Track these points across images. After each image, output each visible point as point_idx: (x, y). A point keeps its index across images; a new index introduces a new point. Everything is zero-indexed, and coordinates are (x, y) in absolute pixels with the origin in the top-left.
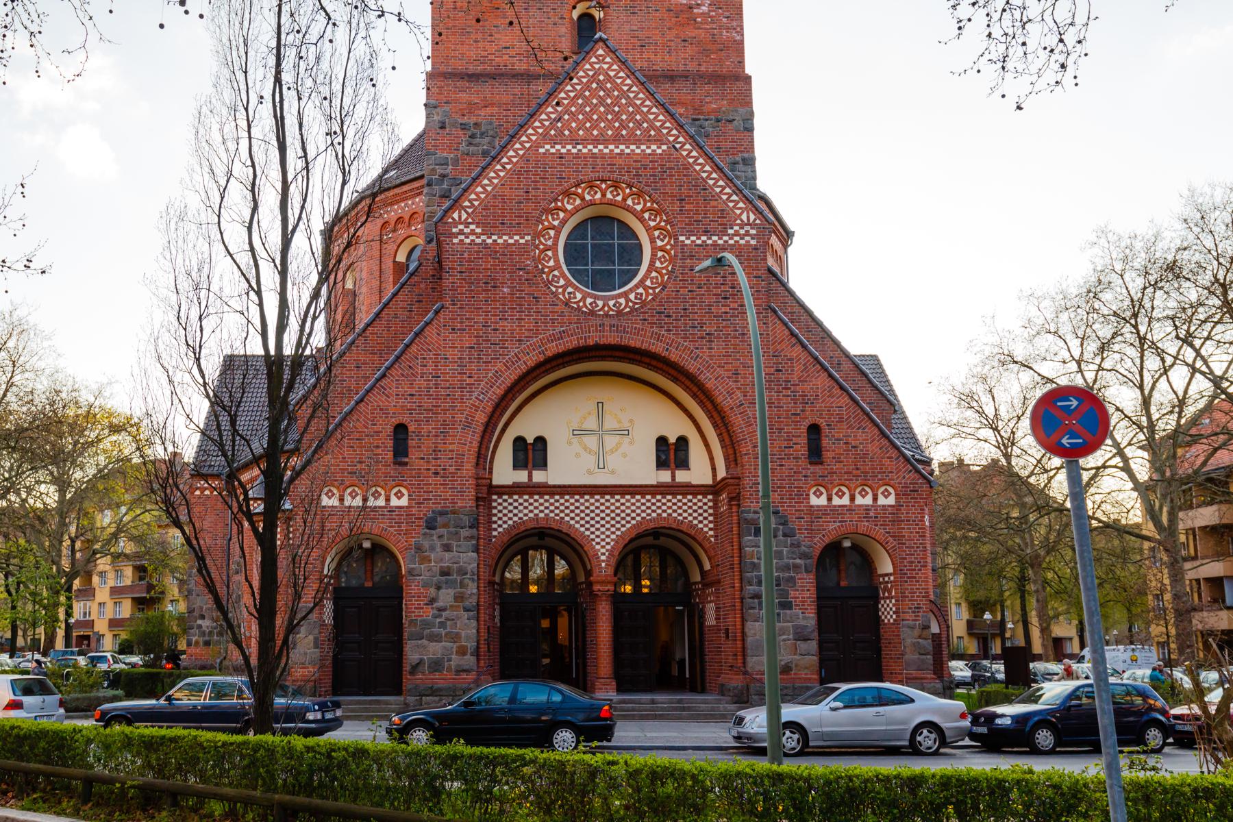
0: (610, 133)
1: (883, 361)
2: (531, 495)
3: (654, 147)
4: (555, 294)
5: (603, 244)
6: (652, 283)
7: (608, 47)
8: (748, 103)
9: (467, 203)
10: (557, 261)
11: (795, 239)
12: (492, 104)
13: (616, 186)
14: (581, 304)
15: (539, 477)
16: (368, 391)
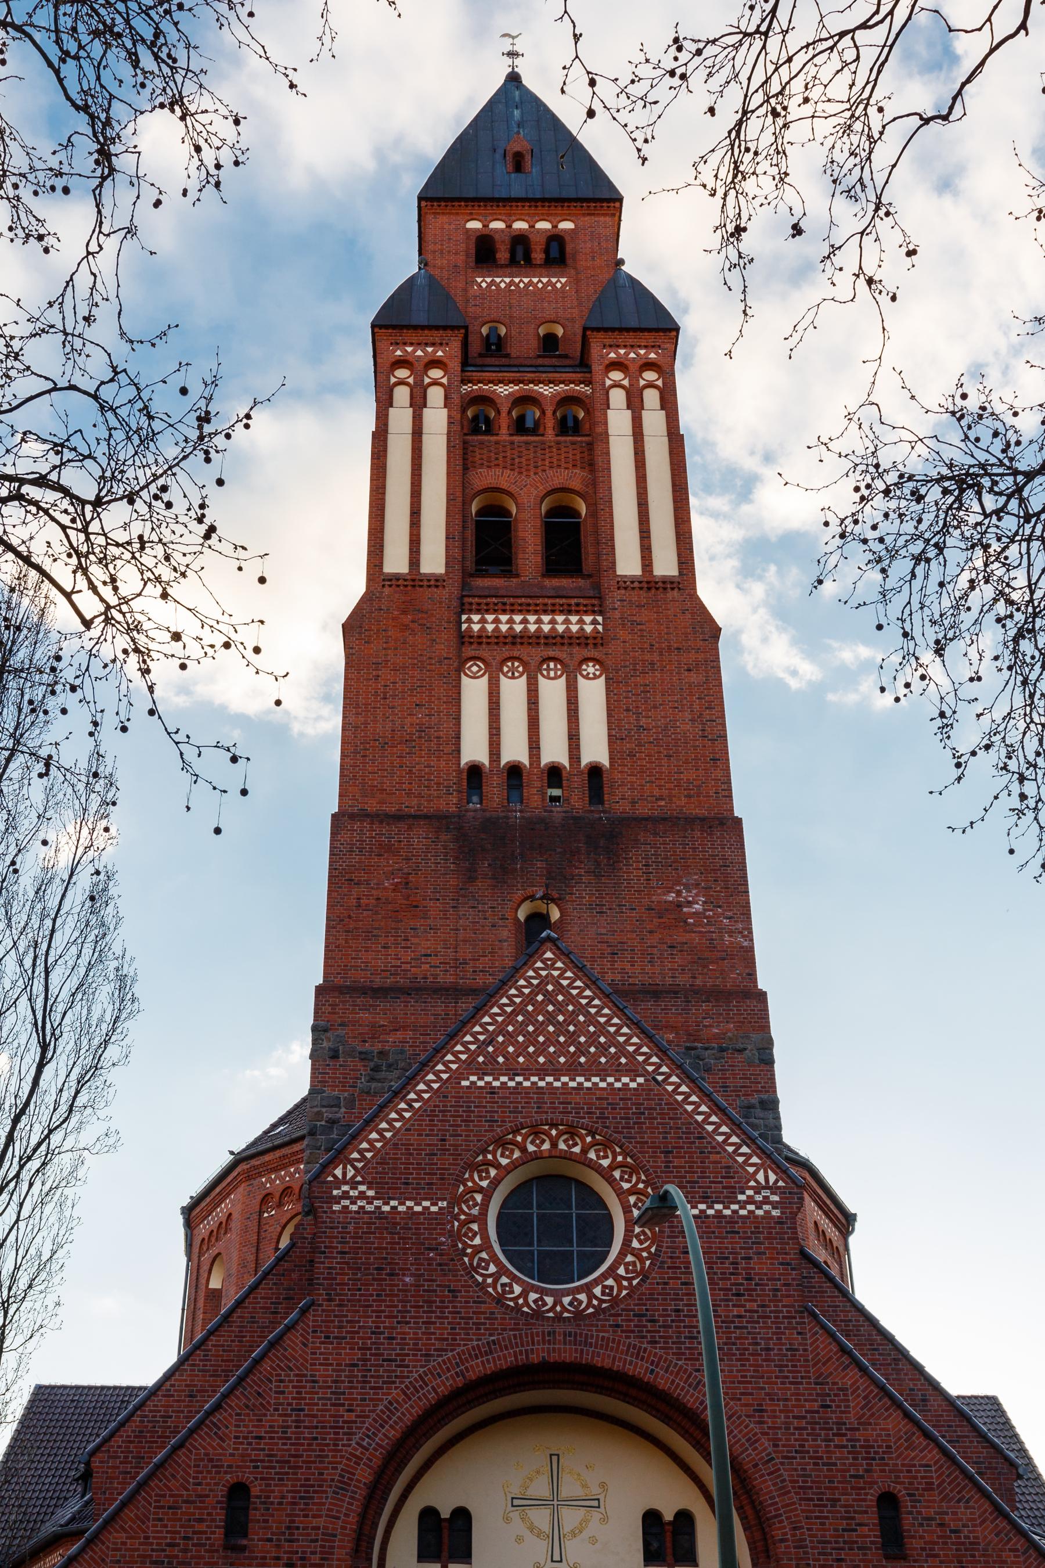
0: (562, 1060)
1: (1006, 1406)
3: (625, 1080)
4: (483, 1286)
5: (556, 1215)
6: (627, 1271)
7: (559, 948)
8: (764, 1026)
9: (355, 1155)
10: (485, 1237)
11: (857, 1225)
12: (405, 1028)
13: (572, 1132)
14: (521, 1301)
16: (192, 1431)
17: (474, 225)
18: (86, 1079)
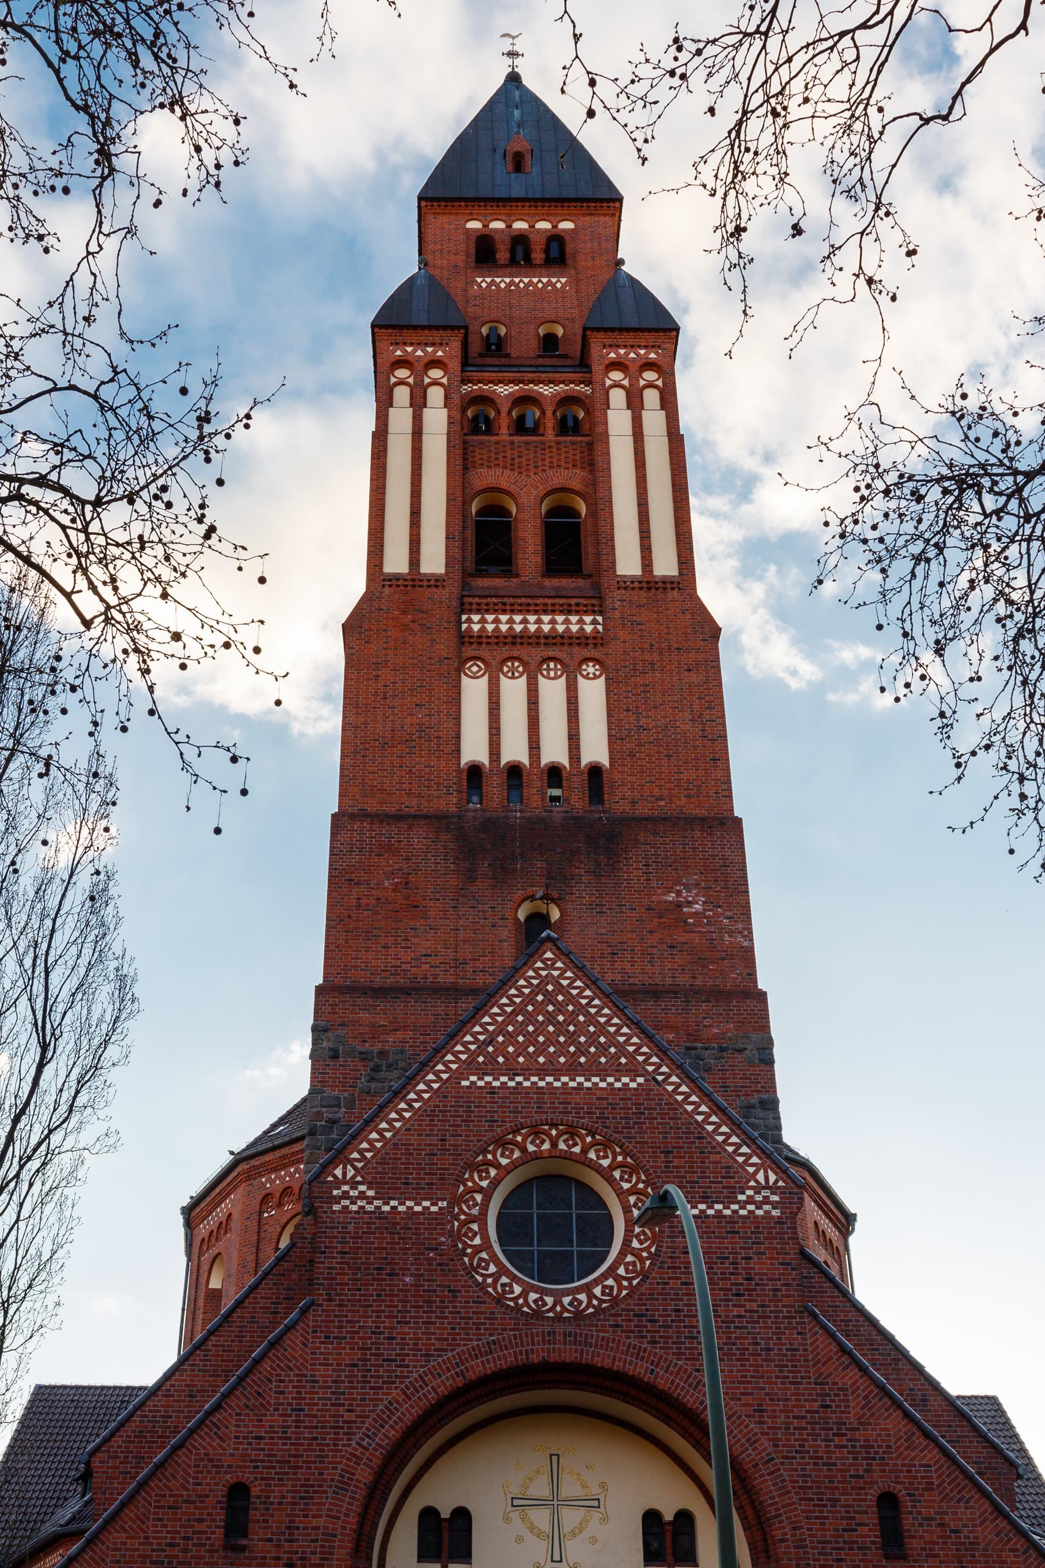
0: (562, 1060)
1: (1006, 1406)
3: (625, 1080)
4: (483, 1286)
5: (556, 1215)
6: (627, 1271)
7: (559, 948)
8: (764, 1026)
9: (355, 1155)
10: (485, 1237)
11: (857, 1225)
12: (405, 1028)
13: (572, 1132)
14: (521, 1301)
16: (192, 1431)
17: (474, 225)
18: (86, 1079)
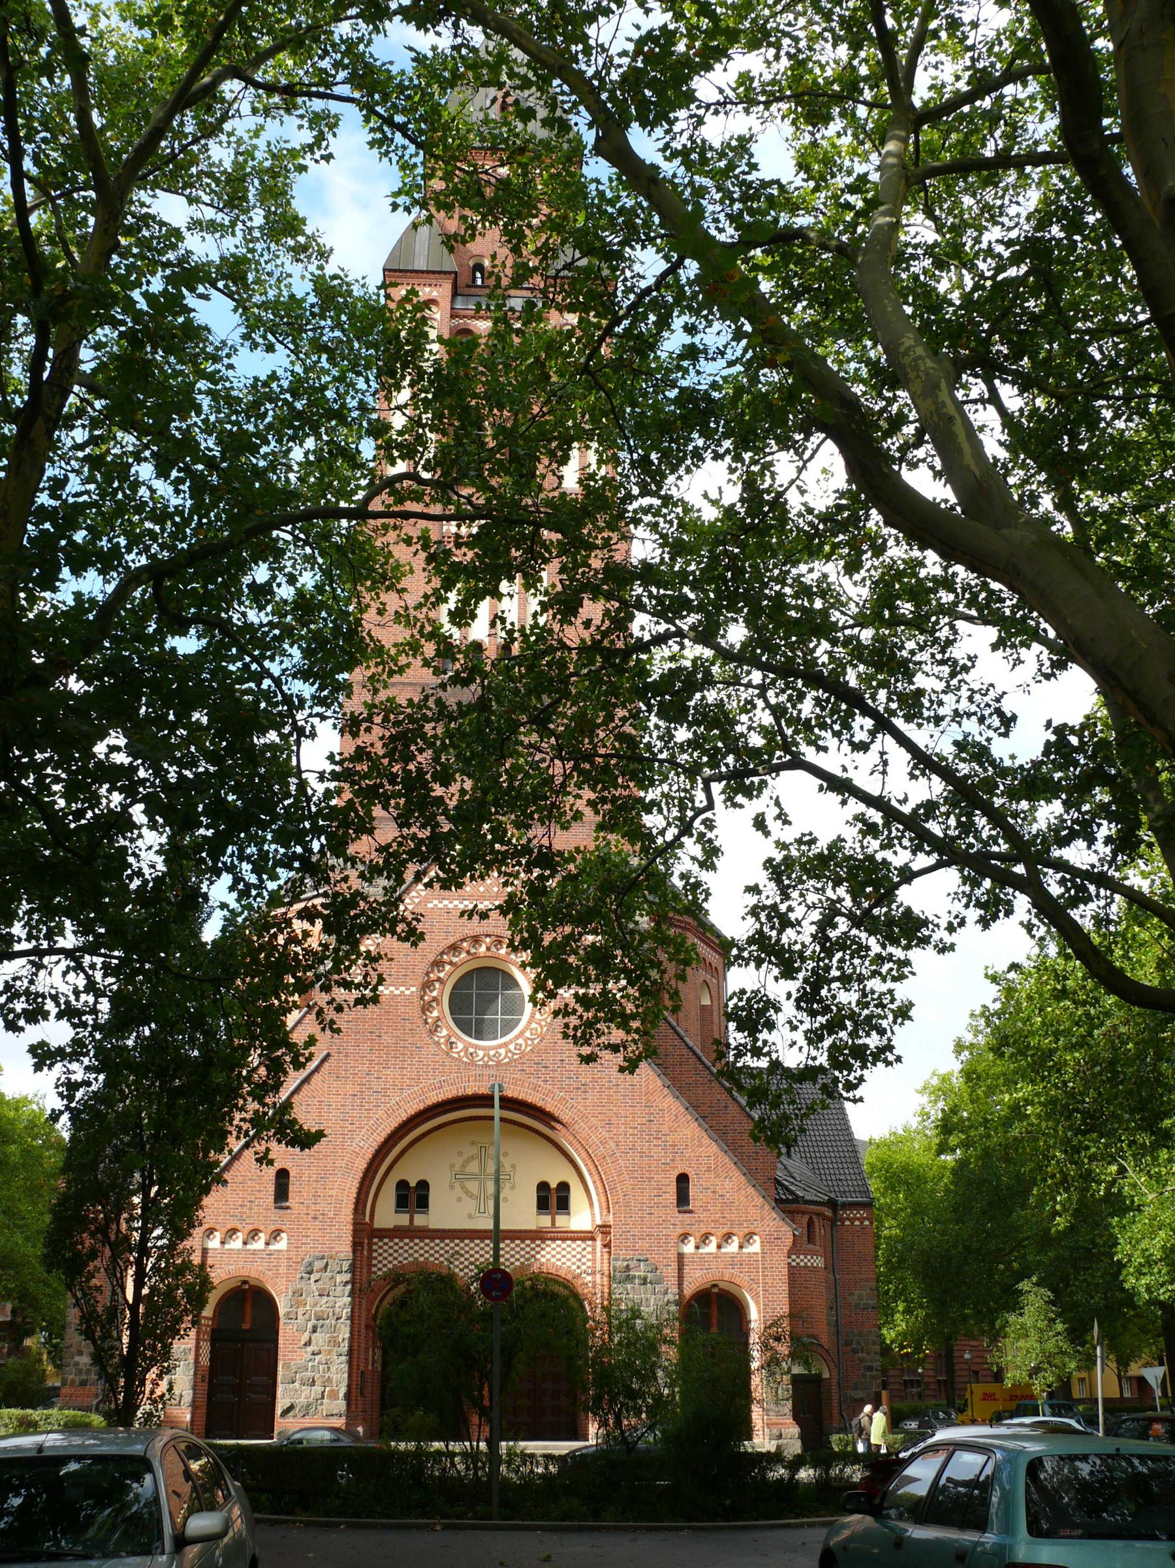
2: (412, 1239)
15: (420, 1220)
